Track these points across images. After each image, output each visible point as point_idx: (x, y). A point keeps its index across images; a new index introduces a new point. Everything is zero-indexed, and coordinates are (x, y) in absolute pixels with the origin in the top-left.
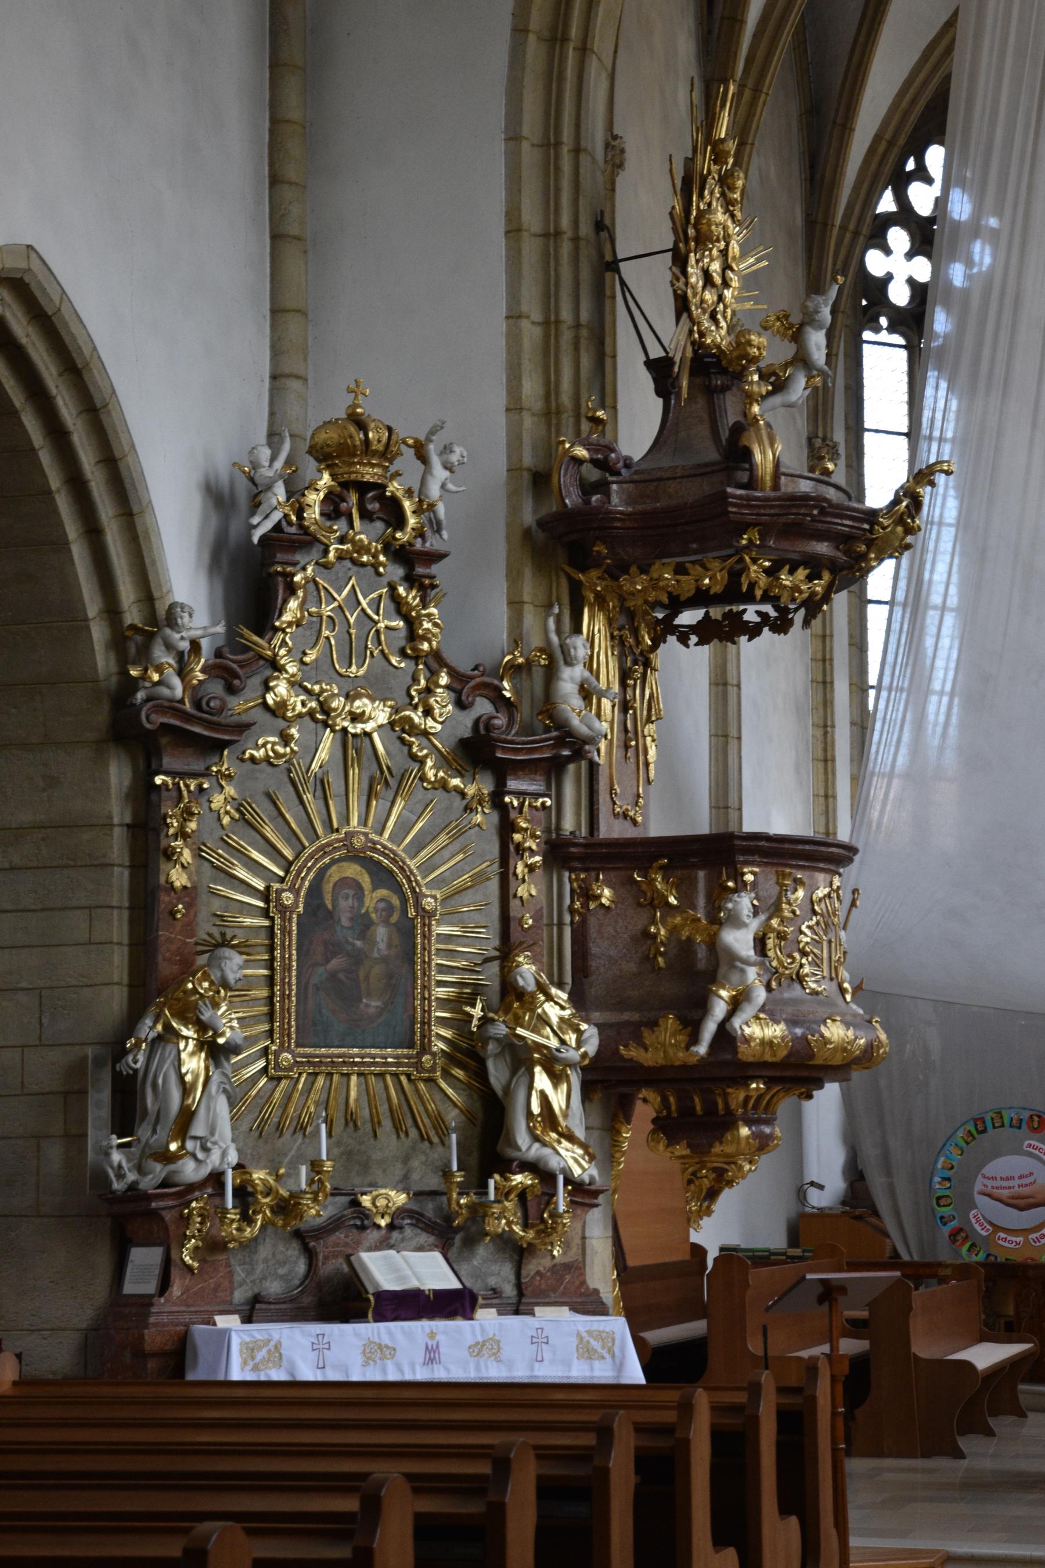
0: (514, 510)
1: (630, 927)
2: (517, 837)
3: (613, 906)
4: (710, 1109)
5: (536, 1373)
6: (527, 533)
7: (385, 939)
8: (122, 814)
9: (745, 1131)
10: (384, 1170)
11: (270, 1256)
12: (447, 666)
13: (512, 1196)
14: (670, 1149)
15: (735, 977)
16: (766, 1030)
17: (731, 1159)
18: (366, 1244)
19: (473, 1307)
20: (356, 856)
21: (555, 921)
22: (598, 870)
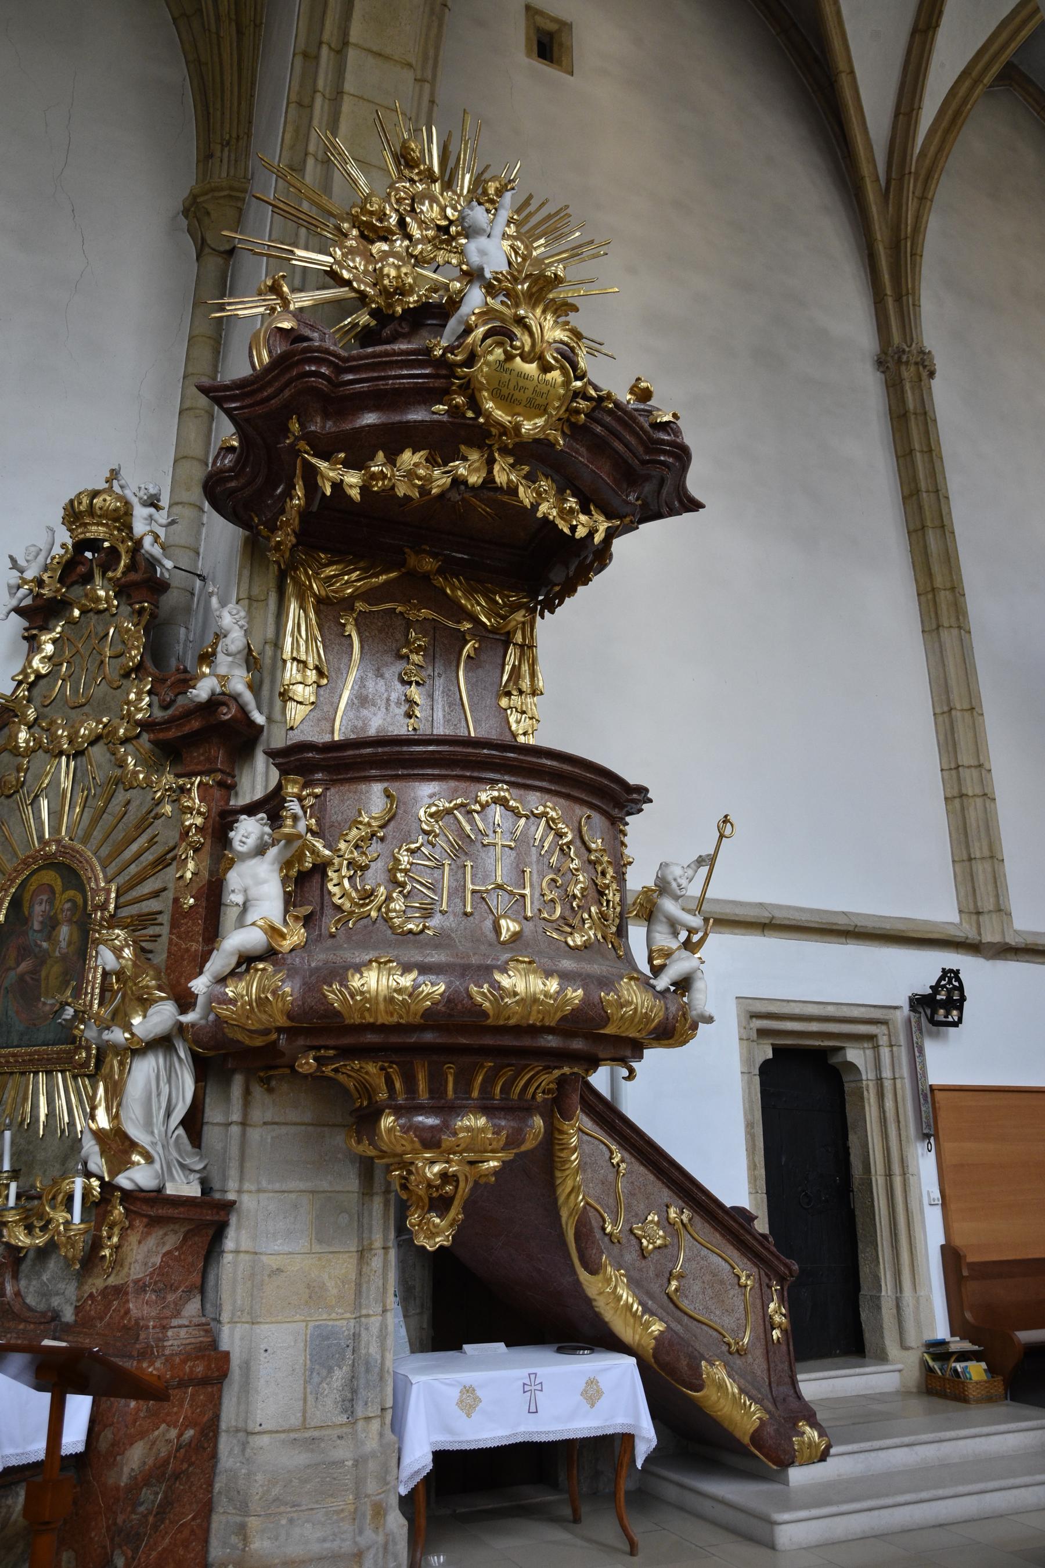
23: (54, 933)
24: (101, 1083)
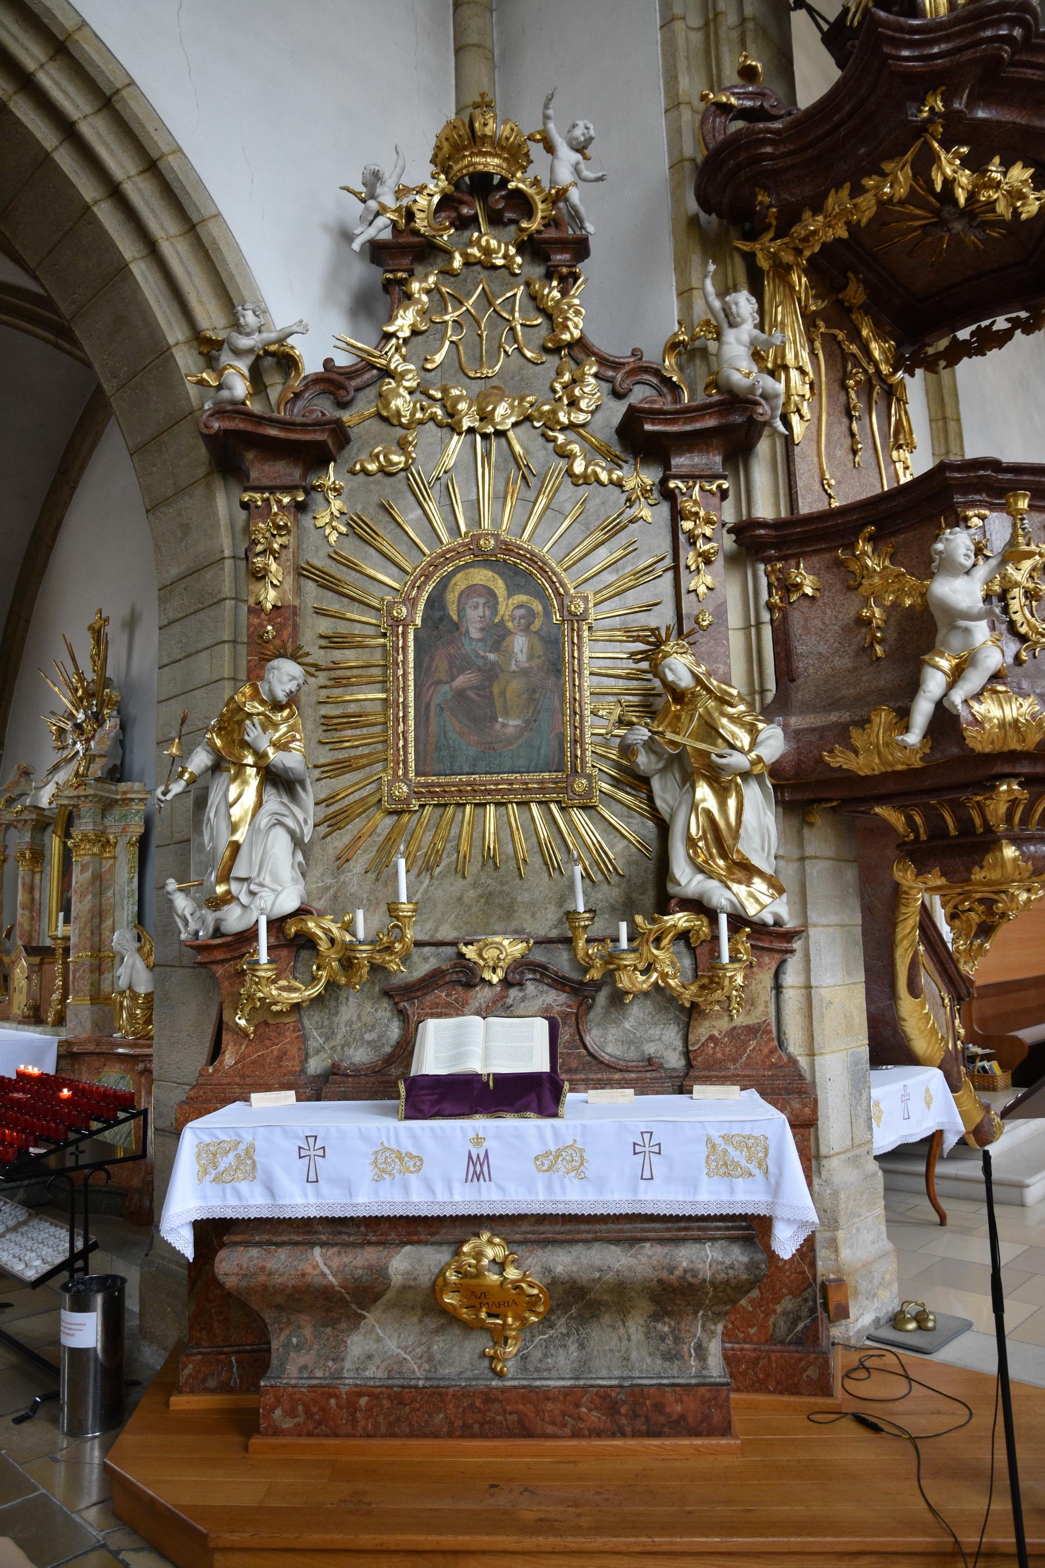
0: (677, 200)
1: (841, 616)
2: (687, 525)
3: (818, 594)
4: (966, 827)
5: (642, 1197)
6: (693, 221)
7: (525, 650)
8: (234, 545)
9: (1010, 852)
10: (533, 915)
11: (354, 1019)
12: (595, 354)
13: (665, 942)
14: (920, 879)
15: (956, 641)
16: (1007, 708)
17: (1003, 888)
18: (475, 1004)
19: (557, 1096)
20: (484, 559)
21: (753, 622)
22: (797, 556)
23: (504, 644)
24: (878, 810)
